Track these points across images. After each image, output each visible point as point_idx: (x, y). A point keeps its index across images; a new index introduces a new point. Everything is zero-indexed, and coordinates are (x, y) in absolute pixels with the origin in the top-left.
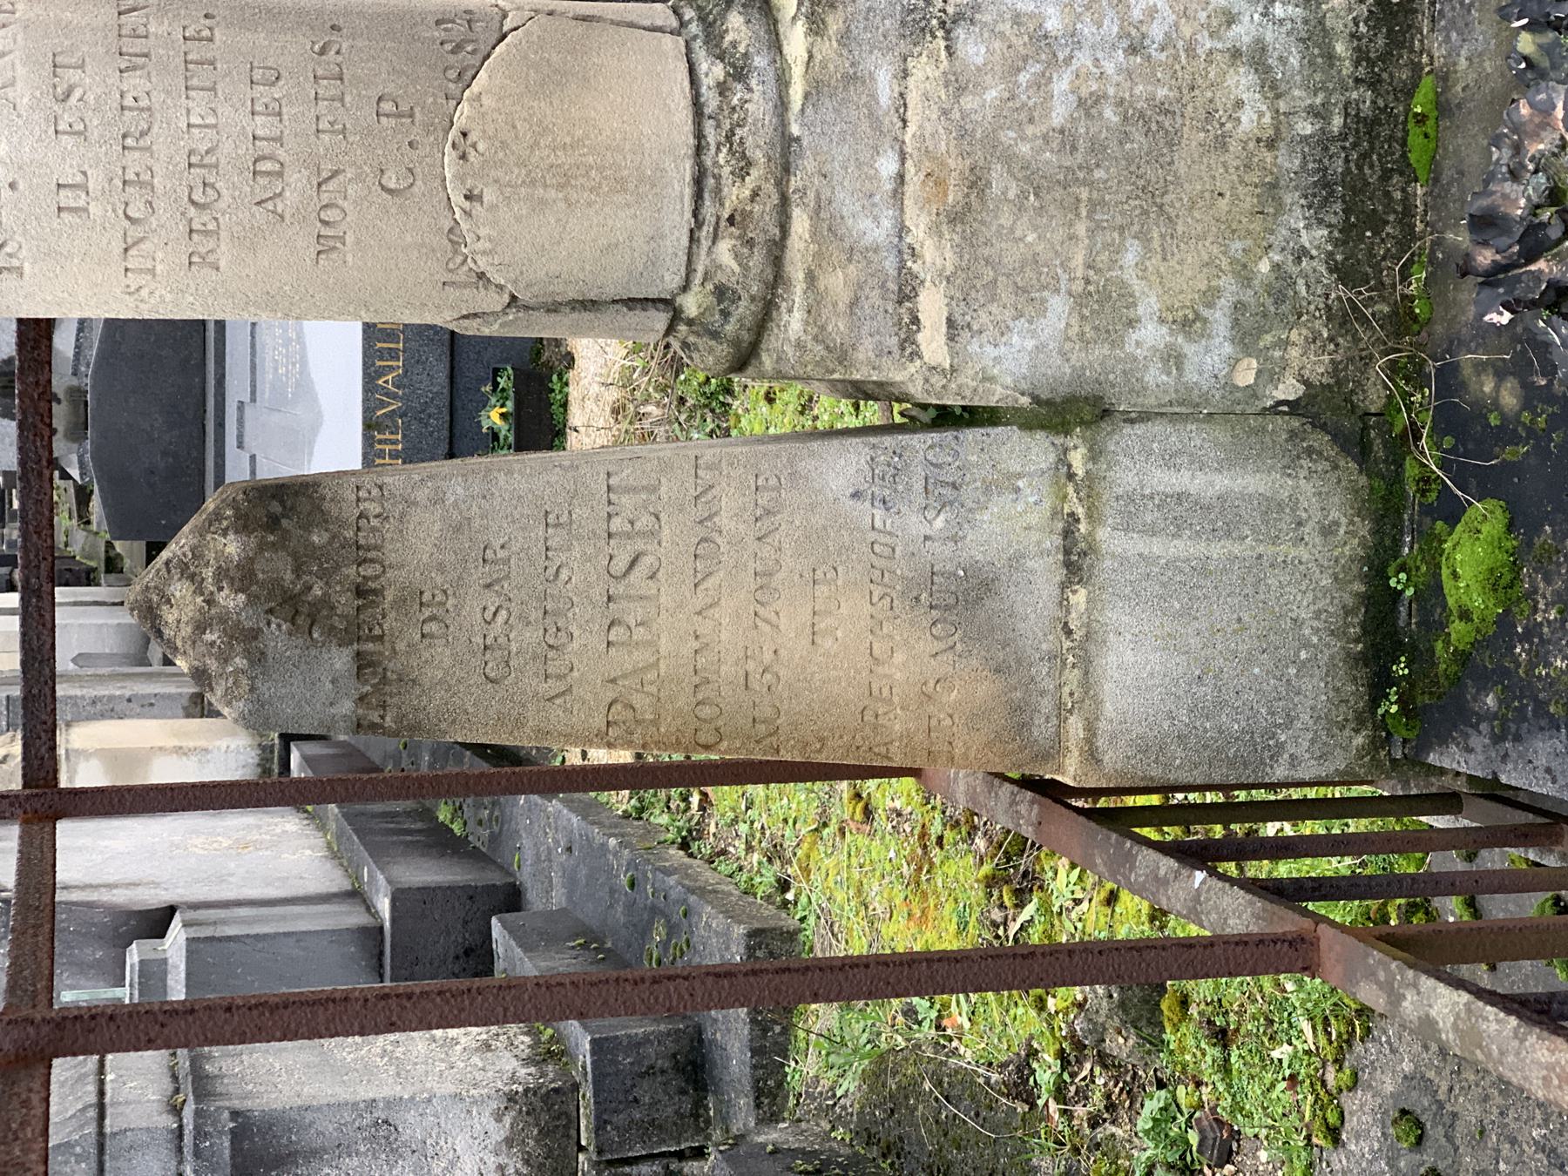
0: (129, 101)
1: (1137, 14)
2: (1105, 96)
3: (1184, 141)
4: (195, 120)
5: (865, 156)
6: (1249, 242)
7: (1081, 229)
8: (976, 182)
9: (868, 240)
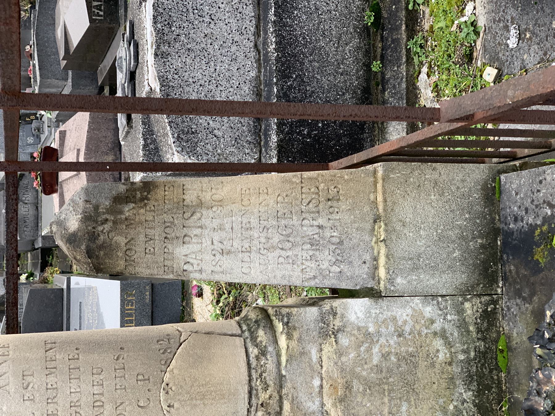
0: (49, 386)
1: (400, 323)
2: (391, 352)
3: (420, 366)
4: (72, 390)
5: (308, 380)
6: (445, 399)
7: (386, 400)
8: (348, 387)
9: (311, 409)
